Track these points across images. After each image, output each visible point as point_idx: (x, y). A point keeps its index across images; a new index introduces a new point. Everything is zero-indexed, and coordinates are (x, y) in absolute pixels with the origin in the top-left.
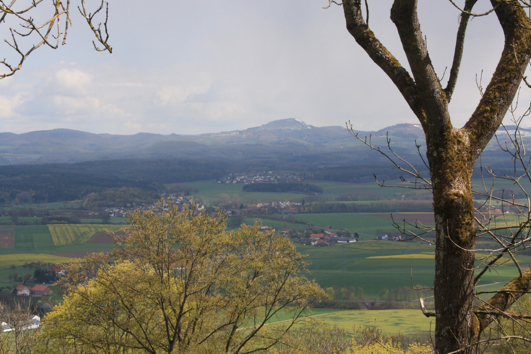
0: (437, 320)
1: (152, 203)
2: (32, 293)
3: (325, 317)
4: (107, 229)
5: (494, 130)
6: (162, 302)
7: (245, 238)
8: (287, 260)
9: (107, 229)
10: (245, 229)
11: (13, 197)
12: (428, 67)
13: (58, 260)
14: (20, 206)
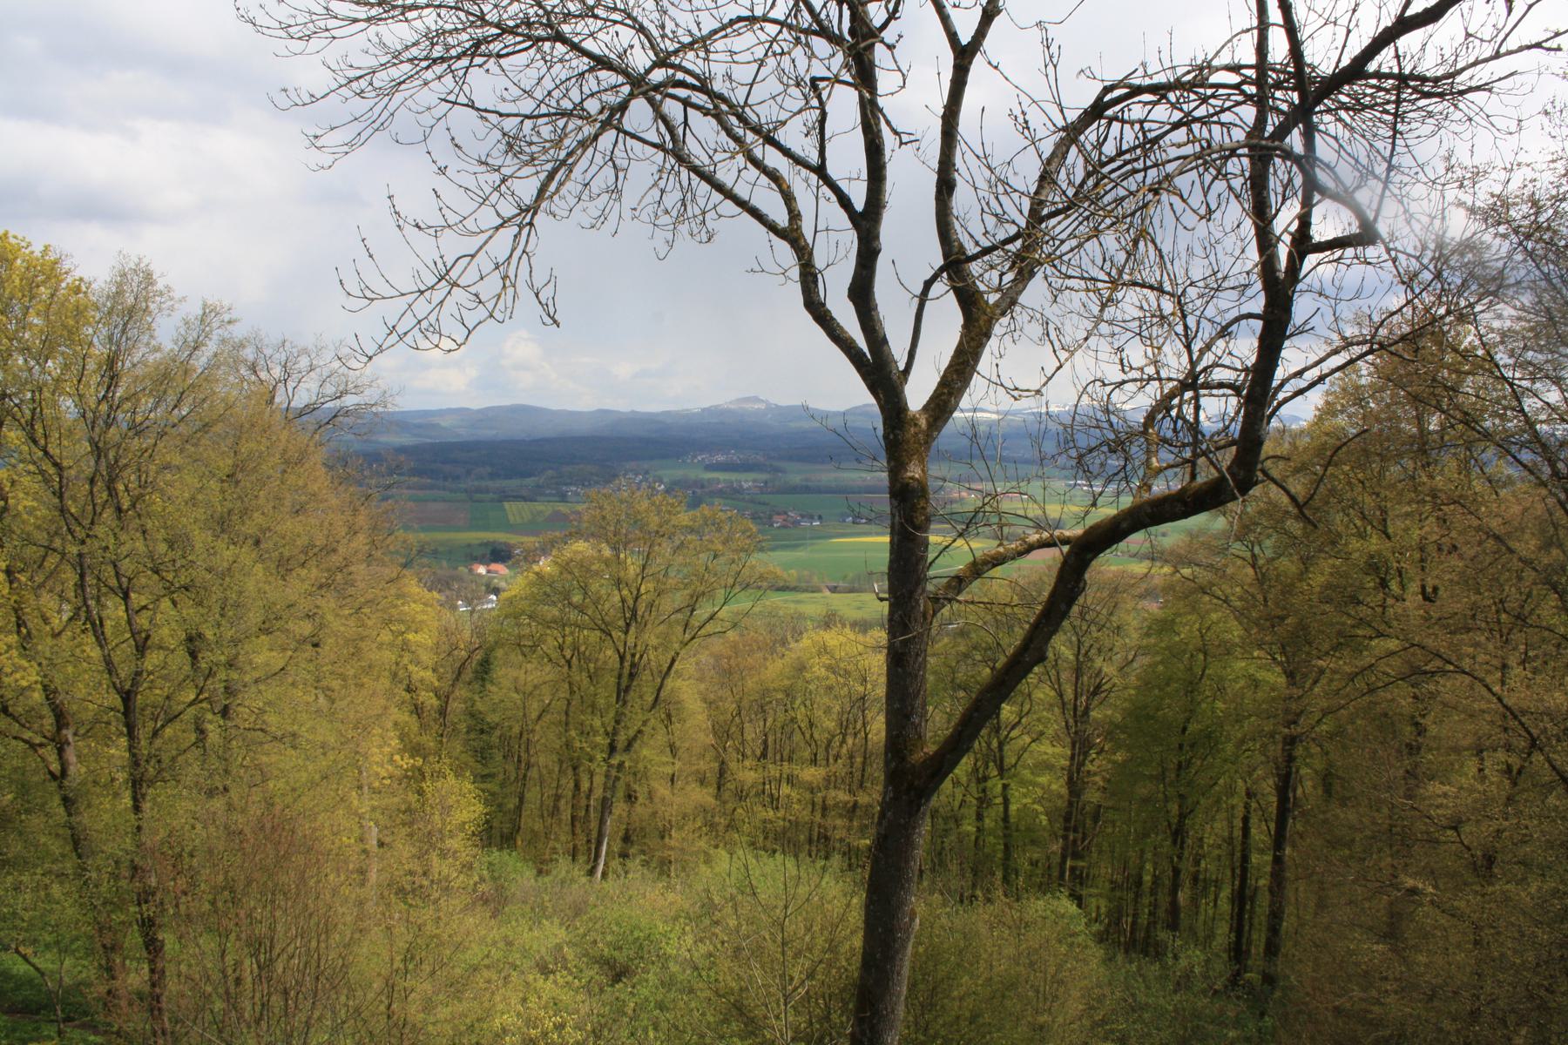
0: (890, 606)
1: (611, 482)
2: (489, 572)
3: (786, 601)
4: (563, 508)
5: (952, 413)
6: (618, 583)
7: (705, 519)
8: (748, 542)
9: (563, 508)
10: (705, 510)
11: (469, 473)
12: (885, 348)
13: (512, 539)
14: (476, 483)
